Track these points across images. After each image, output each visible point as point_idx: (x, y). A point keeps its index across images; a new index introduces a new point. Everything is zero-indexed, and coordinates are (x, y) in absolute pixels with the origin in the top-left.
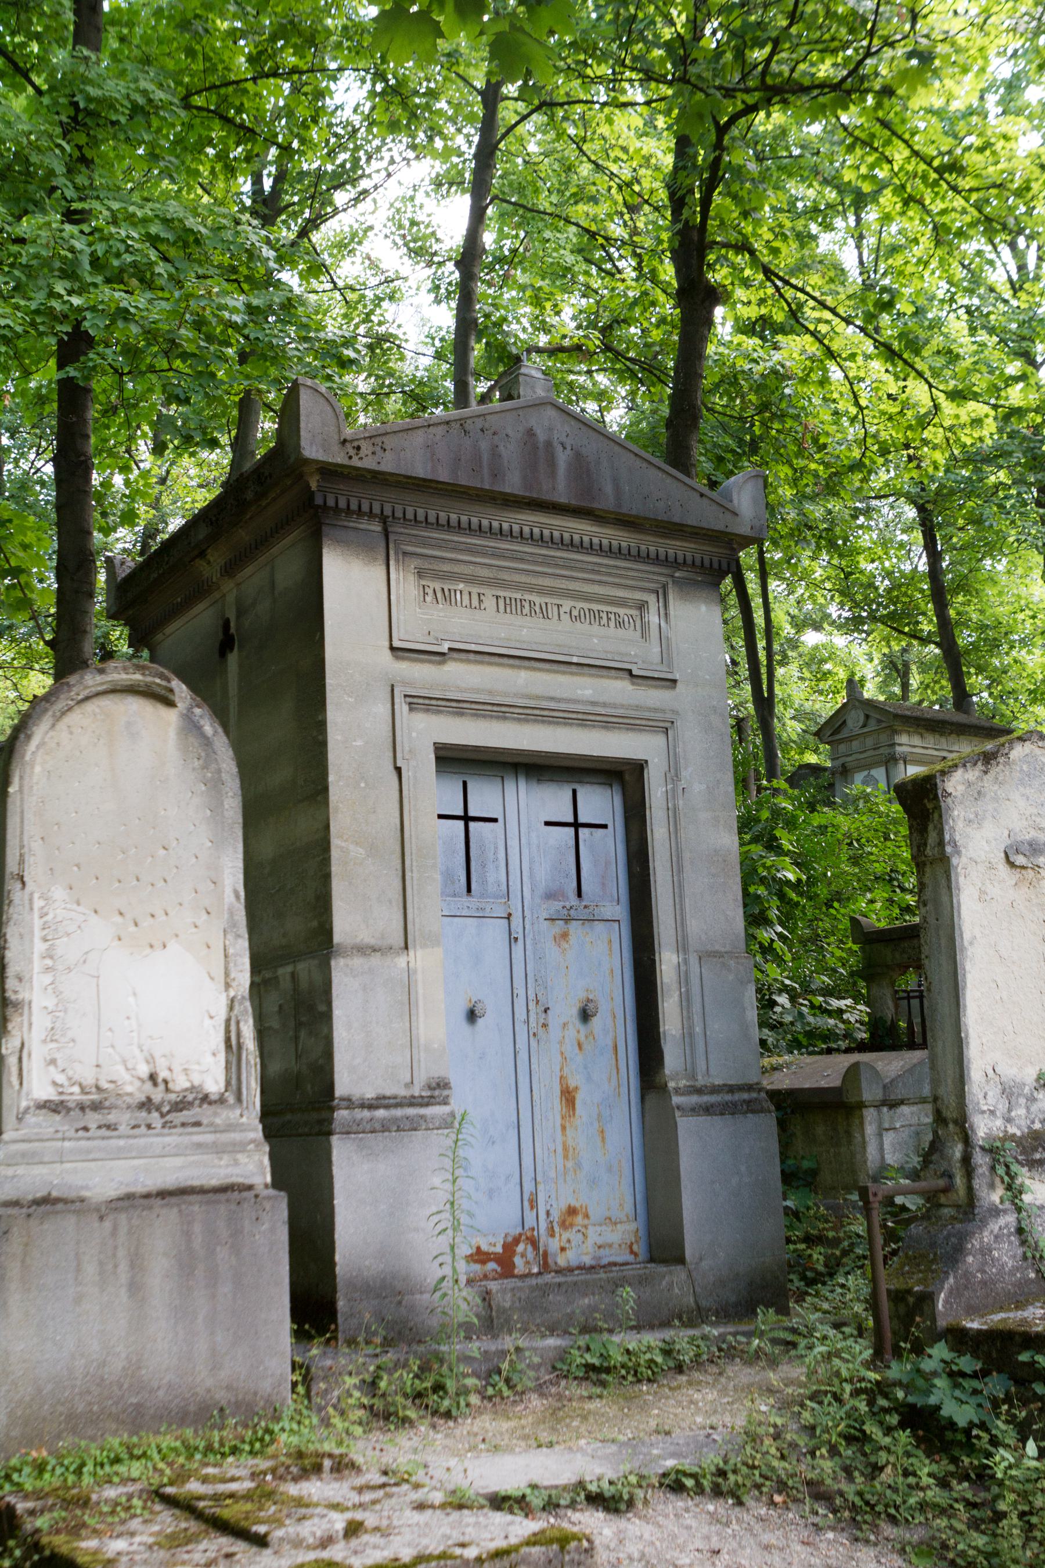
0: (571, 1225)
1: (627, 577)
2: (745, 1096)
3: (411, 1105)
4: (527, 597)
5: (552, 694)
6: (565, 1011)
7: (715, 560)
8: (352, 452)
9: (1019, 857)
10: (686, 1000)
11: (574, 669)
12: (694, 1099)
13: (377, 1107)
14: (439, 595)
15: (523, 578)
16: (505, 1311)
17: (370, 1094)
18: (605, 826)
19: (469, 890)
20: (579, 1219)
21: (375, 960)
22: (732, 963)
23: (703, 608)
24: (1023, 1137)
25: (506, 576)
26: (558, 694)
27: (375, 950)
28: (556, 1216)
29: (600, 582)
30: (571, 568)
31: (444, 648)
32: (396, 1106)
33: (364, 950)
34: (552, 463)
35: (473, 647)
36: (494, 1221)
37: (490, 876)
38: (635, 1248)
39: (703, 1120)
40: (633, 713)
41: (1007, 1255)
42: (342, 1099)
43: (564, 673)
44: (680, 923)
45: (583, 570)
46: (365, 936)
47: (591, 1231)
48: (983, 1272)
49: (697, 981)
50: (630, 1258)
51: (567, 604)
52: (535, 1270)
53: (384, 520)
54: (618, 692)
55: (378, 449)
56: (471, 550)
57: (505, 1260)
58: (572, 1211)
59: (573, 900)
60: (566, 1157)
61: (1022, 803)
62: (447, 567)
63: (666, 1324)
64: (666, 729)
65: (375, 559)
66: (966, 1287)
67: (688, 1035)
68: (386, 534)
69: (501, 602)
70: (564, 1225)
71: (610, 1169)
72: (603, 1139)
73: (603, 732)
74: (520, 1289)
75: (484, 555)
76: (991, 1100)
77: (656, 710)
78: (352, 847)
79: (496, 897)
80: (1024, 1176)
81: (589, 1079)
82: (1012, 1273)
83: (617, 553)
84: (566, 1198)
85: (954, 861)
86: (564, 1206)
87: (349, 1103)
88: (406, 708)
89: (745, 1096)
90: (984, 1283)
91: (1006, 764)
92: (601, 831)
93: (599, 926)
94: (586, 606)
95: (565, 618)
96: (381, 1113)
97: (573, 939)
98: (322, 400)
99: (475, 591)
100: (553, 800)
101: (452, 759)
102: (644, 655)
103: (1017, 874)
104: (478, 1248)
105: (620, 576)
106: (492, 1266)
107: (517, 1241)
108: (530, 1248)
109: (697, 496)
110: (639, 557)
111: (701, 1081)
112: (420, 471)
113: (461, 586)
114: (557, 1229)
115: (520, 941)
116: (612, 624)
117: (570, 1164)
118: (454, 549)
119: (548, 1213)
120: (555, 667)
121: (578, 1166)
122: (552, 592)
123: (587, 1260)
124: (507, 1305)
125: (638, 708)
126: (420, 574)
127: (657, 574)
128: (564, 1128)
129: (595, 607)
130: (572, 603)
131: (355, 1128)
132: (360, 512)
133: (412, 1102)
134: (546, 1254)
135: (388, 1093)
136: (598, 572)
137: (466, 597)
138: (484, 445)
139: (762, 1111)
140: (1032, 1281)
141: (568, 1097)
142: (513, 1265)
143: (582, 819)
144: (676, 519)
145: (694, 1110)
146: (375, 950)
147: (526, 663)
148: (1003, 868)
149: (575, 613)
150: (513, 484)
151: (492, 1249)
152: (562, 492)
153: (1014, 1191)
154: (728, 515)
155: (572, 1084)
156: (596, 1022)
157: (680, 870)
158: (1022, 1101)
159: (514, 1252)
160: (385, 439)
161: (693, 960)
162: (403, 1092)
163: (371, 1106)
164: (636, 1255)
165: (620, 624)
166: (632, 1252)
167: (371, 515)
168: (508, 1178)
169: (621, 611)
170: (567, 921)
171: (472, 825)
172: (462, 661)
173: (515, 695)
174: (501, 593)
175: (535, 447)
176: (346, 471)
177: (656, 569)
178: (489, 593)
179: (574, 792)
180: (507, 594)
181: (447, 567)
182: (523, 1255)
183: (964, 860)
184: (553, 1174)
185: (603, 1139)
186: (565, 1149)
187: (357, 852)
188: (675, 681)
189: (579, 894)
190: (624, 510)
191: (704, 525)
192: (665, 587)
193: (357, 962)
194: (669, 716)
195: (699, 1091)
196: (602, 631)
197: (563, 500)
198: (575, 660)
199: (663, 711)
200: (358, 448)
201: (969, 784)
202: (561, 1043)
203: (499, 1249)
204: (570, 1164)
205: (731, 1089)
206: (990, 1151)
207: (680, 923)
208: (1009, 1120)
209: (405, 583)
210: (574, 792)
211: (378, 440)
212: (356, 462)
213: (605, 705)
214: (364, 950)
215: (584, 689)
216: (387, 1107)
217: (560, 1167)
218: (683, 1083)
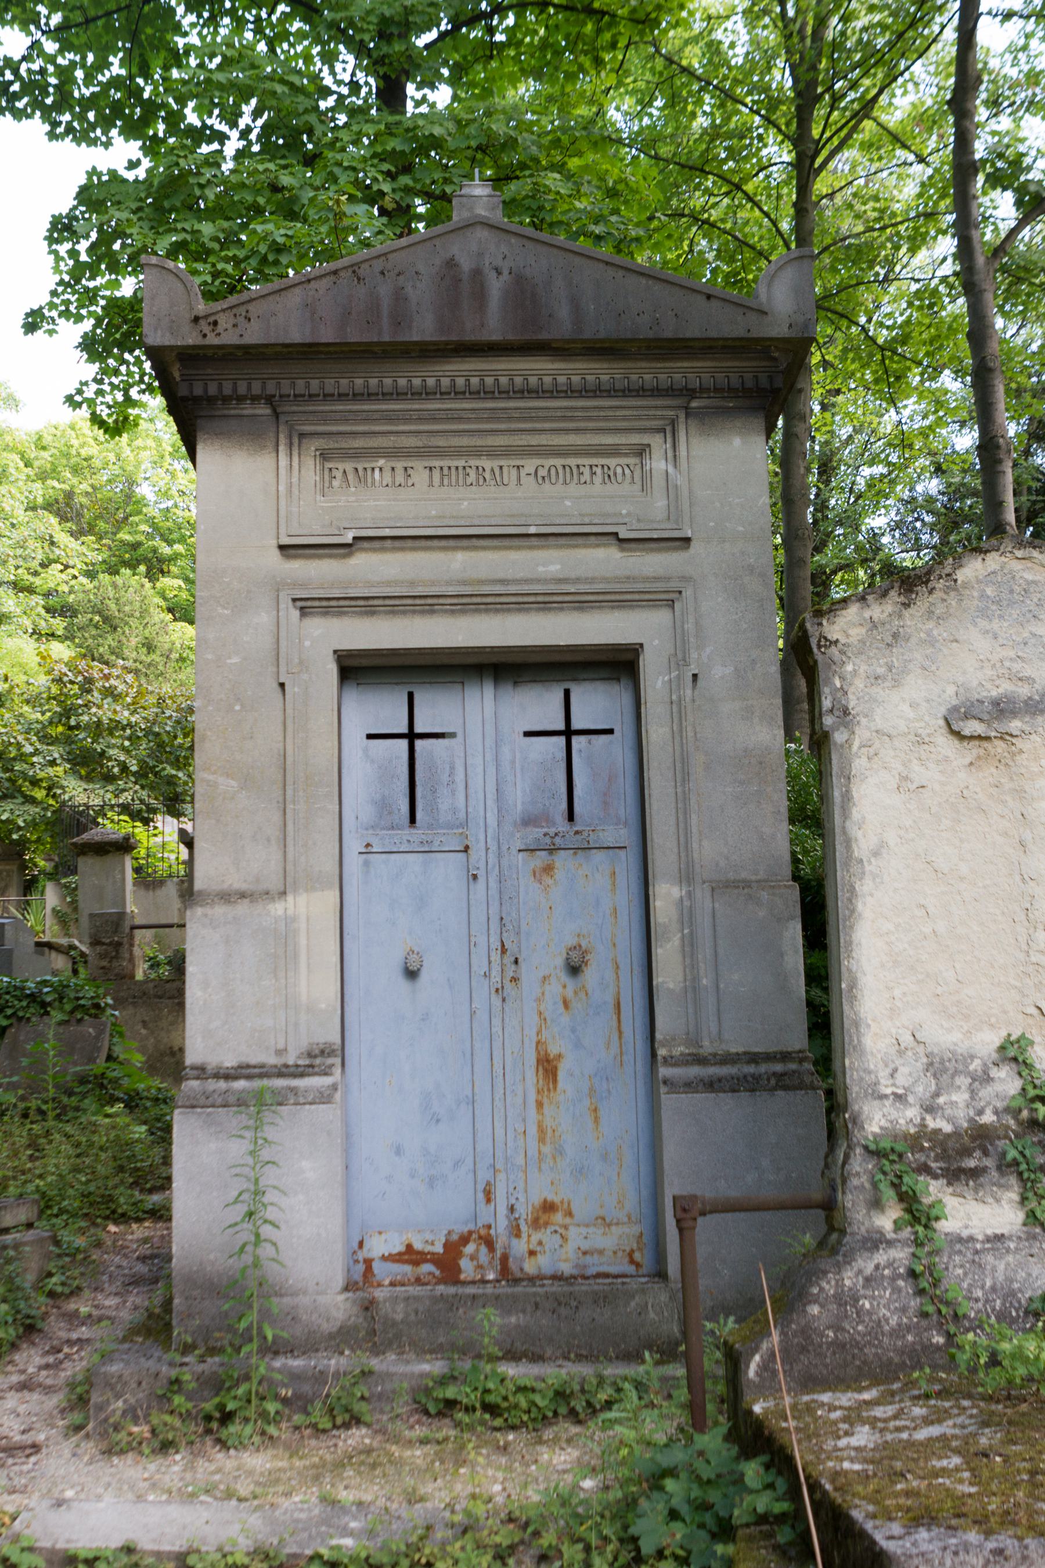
0: (546, 1224)
1: (615, 419)
2: (778, 1068)
3: (280, 1075)
4: (473, 462)
5: (501, 575)
6: (543, 960)
7: (748, 377)
8: (207, 329)
9: (980, 723)
10: (690, 946)
11: (534, 541)
12: (694, 1071)
13: (236, 1078)
14: (351, 476)
15: (465, 441)
16: (394, 1324)
17: (229, 1062)
18: (610, 731)
19: (413, 820)
20: (558, 1217)
21: (242, 908)
22: (764, 895)
23: (737, 441)
24: (956, 1134)
25: (441, 442)
26: (509, 575)
27: (243, 895)
28: (523, 1211)
29: (577, 431)
30: (531, 419)
31: (348, 538)
32: (261, 1076)
33: (227, 897)
34: (480, 295)
35: (387, 532)
36: (415, 1212)
37: (442, 802)
38: (637, 1256)
39: (702, 1099)
40: (618, 587)
41: (888, 1308)
42: (193, 1068)
43: (519, 548)
44: (684, 845)
45: (546, 419)
46: (235, 881)
47: (573, 1232)
48: (838, 1329)
49: (707, 921)
50: (631, 1269)
51: (530, 465)
52: (491, 1276)
53: (269, 400)
54: (602, 562)
55: (241, 320)
56: (389, 418)
57: (447, 1263)
58: (549, 1207)
59: (561, 824)
60: (542, 1140)
61: (983, 645)
62: (358, 443)
63: (634, 1357)
64: (667, 598)
65: (263, 447)
66: (804, 1349)
67: (692, 988)
68: (276, 415)
69: (436, 474)
70: (536, 1224)
71: (605, 1157)
72: (596, 1120)
73: (576, 615)
74: (417, 1299)
75: (407, 421)
76: (902, 1079)
77: (657, 579)
78: (221, 780)
79: (450, 826)
80: (934, 1190)
81: (578, 1045)
82: (898, 1332)
83: (597, 391)
84: (540, 1191)
85: (839, 737)
86: (536, 1199)
87: (201, 1071)
88: (296, 613)
89: (778, 1068)
90: (839, 1346)
91: (947, 590)
92: (603, 738)
93: (598, 856)
94: (559, 462)
95: (528, 482)
96: (241, 1084)
97: (559, 874)
98: (171, 277)
99: (399, 465)
100: (541, 705)
101: (356, 669)
102: (653, 512)
103: (973, 750)
104: (409, 1247)
105: (606, 419)
106: (427, 1268)
107: (465, 1240)
108: (484, 1249)
109: (701, 300)
110: (641, 392)
111: (707, 1047)
112: (296, 336)
113: (381, 462)
114: (524, 1228)
115: (482, 880)
116: (597, 480)
117: (547, 1149)
118: (366, 420)
119: (512, 1209)
120: (507, 542)
121: (559, 1151)
122: (508, 452)
123: (566, 1268)
124: (399, 1317)
125: (628, 579)
126: (324, 456)
127: (661, 409)
128: (540, 1105)
129: (572, 462)
130: (538, 462)
131: (202, 1101)
132: (241, 399)
133: (283, 1072)
134: (505, 1259)
135: (253, 1060)
136: (572, 419)
137: (387, 474)
138: (385, 291)
139: (801, 1086)
140: (938, 1348)
141: (548, 1067)
142: (459, 1271)
143: (576, 725)
144: (669, 334)
145: (689, 1086)
146: (243, 895)
147: (465, 543)
148: (946, 745)
149: (542, 472)
150: (424, 328)
151: (429, 1248)
152: (494, 325)
153: (919, 1215)
154: (752, 317)
155: (553, 1050)
156: (590, 975)
157: (686, 777)
158: (963, 1081)
159: (460, 1254)
160: (251, 307)
161: (702, 894)
162: (272, 1060)
163: (228, 1076)
164: (638, 1265)
165: (609, 477)
166: (632, 1261)
167: (255, 399)
168: (457, 1164)
169: (612, 462)
170: (552, 850)
171: (419, 744)
172: (374, 550)
173: (449, 583)
174: (437, 463)
175: (457, 281)
176: (210, 353)
177: (659, 402)
178: (418, 465)
179: (567, 694)
180: (445, 463)
181: (358, 443)
182: (473, 1258)
183: (862, 734)
184: (520, 1160)
185: (596, 1120)
186: (541, 1130)
187: (228, 784)
188: (687, 540)
189: (571, 817)
190: (587, 335)
191: (714, 334)
192: (673, 423)
193: (219, 911)
194: (674, 585)
195: (700, 1060)
196: (583, 490)
197: (496, 337)
198: (532, 530)
199: (668, 579)
200: (215, 323)
201: (874, 625)
202: (538, 1000)
203: (439, 1249)
204: (547, 1149)
205: (754, 1058)
206: (875, 1153)
207: (684, 845)
208: (930, 1109)
209: (307, 470)
210: (567, 694)
211: (242, 310)
212: (212, 340)
213: (577, 580)
214: (227, 897)
215: (549, 564)
216: (249, 1077)
217: (533, 1151)
218: (679, 1050)
